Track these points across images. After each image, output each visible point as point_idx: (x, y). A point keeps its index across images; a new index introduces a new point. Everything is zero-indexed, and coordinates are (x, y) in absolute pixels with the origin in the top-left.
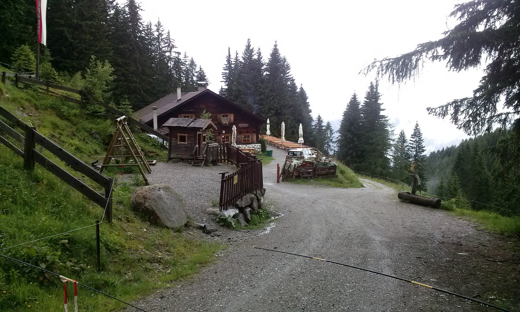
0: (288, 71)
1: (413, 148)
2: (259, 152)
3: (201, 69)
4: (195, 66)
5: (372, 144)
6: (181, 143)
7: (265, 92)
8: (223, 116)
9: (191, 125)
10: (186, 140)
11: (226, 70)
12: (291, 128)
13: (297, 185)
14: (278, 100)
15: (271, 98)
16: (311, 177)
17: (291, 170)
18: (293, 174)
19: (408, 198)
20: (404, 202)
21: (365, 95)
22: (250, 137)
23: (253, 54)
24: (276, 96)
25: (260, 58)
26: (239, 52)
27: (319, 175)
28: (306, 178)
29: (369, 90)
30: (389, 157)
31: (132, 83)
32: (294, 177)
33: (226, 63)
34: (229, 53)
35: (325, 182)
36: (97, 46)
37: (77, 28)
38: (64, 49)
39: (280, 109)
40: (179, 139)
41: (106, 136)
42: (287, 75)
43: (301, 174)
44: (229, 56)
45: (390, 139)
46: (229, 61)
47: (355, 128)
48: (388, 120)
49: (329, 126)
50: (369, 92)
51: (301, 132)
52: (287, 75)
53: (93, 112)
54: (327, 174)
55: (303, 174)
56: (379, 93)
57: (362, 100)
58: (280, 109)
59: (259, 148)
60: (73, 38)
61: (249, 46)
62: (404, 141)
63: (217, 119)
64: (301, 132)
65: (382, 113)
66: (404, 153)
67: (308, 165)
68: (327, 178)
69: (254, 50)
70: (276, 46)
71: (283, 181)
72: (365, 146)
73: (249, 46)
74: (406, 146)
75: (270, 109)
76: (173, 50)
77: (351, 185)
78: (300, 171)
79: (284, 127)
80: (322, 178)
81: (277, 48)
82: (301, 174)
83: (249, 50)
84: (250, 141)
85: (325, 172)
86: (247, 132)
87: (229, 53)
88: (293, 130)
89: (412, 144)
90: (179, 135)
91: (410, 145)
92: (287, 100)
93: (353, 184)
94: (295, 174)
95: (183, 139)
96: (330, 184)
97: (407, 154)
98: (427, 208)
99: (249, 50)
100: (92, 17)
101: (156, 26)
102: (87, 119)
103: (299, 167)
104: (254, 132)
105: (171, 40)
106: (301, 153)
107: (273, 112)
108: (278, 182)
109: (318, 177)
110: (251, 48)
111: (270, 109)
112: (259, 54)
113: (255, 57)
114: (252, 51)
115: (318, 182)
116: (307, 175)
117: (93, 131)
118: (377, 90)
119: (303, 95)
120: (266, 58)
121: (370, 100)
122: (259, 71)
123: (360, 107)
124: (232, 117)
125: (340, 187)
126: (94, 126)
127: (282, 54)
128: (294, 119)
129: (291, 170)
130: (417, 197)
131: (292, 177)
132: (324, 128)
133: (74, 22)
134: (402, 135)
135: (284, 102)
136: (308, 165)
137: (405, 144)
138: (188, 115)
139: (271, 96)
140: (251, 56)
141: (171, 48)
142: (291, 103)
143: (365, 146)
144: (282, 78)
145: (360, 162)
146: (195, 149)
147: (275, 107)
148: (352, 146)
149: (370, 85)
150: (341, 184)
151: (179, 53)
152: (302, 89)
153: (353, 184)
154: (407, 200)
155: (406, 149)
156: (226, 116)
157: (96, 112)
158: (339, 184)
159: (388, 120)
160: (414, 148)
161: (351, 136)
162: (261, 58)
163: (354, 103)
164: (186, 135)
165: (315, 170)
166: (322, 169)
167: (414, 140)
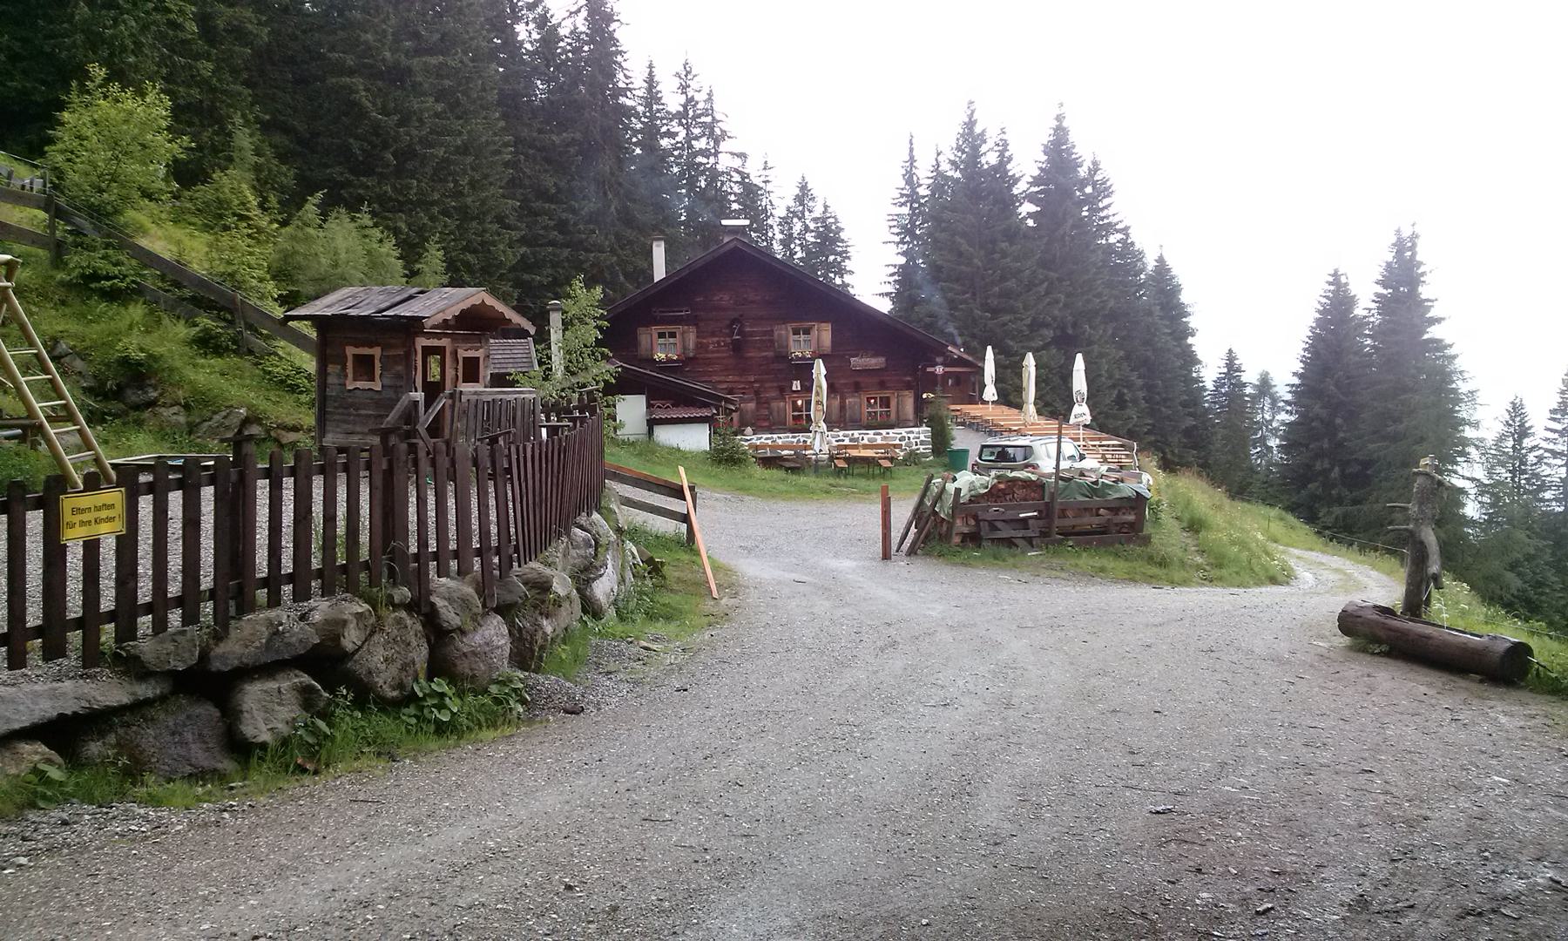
0: (1106, 202)
1: (1555, 454)
2: (925, 455)
3: (826, 207)
4: (813, 199)
5: (1395, 438)
6: (359, 384)
7: (1020, 271)
8: (796, 332)
9: (404, 311)
10: (378, 372)
11: (902, 204)
12: (1114, 386)
13: (963, 569)
14: (1068, 295)
15: (1042, 289)
16: (1029, 540)
17: (944, 511)
18: (951, 525)
19: (1382, 634)
20: (1364, 650)
21: (1377, 273)
22: (893, 403)
23: (983, 149)
24: (1060, 280)
25: (1004, 161)
26: (937, 149)
27: (1067, 534)
28: (1009, 543)
29: (1390, 257)
30: (1459, 483)
31: (587, 250)
32: (957, 540)
33: (902, 184)
34: (911, 150)
35: (1086, 560)
36: (460, 133)
37: (398, 76)
38: (356, 146)
39: (1075, 325)
40: (350, 371)
41: (108, 365)
42: (1102, 214)
43: (985, 527)
44: (912, 160)
45: (1464, 422)
46: (910, 178)
47: (1336, 385)
48: (1454, 357)
49: (1265, 386)
50: (1389, 265)
51: (1079, 383)
52: (1102, 214)
53: (83, 276)
54: (1103, 530)
55: (993, 527)
56: (1420, 264)
57: (1365, 296)
58: (1075, 325)
59: (922, 443)
60: (385, 112)
61: (970, 124)
62: (1523, 432)
63: (772, 341)
64: (1079, 383)
65: (1434, 332)
66: (1524, 472)
67: (1019, 493)
68: (1101, 543)
69: (987, 135)
70: (1059, 118)
71: (912, 552)
72: (1371, 446)
73: (970, 124)
74: (1532, 449)
75: (1036, 325)
76: (723, 146)
77: (1215, 573)
78: (981, 515)
79: (1033, 370)
80: (1078, 544)
81: (1065, 124)
82: (985, 527)
83: (971, 139)
84: (893, 415)
85: (1096, 520)
86: (882, 385)
87: (911, 150)
88: (1120, 396)
89: (1554, 441)
90: (351, 351)
91: (1544, 445)
92: (1099, 295)
93: (1224, 572)
94: (960, 526)
95: (365, 366)
96: (1102, 570)
97: (1537, 476)
98: (1462, 683)
99: (971, 139)
100: (447, 43)
101: (678, 75)
102: (63, 303)
103: (976, 499)
104: (908, 387)
105: (718, 117)
106: (1028, 451)
107: (1049, 333)
108: (886, 556)
109: (1060, 542)
110: (978, 130)
111: (1036, 325)
112: (1003, 147)
113: (990, 159)
114: (982, 138)
115: (1055, 561)
116: (1013, 533)
117: (63, 346)
118: (1414, 255)
119: (1164, 287)
120: (1026, 165)
121: (1396, 289)
122: (1008, 203)
123: (1359, 311)
124: (824, 334)
125: (1150, 580)
126: (73, 327)
127: (1084, 148)
128: (1127, 358)
129: (944, 511)
130: (1429, 630)
131: (945, 538)
132: (1248, 390)
133: (384, 60)
134: (1516, 410)
135: (1088, 301)
136: (1019, 493)
137: (1527, 443)
138: (671, 328)
139: (1042, 282)
140: (975, 155)
141: (717, 142)
142: (1112, 303)
143: (1371, 446)
144: (1081, 223)
145: (1355, 502)
146: (400, 407)
147: (1054, 319)
148: (1326, 446)
149: (1394, 239)
150: (1161, 570)
151: (742, 156)
152: (1161, 260)
153: (1220, 567)
154: (1377, 640)
155: (1531, 458)
156: (807, 332)
157: (95, 277)
158: (1155, 570)
159: (1454, 357)
160: (1561, 454)
161: (1323, 413)
162: (1010, 159)
163: (1338, 304)
164: (376, 352)
165: (1046, 513)
166: (1085, 510)
167: (1559, 427)
